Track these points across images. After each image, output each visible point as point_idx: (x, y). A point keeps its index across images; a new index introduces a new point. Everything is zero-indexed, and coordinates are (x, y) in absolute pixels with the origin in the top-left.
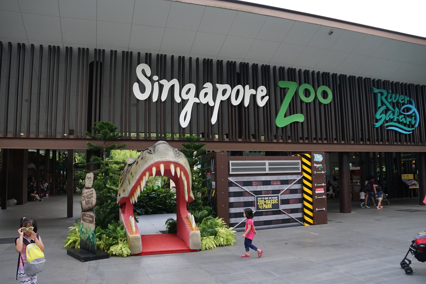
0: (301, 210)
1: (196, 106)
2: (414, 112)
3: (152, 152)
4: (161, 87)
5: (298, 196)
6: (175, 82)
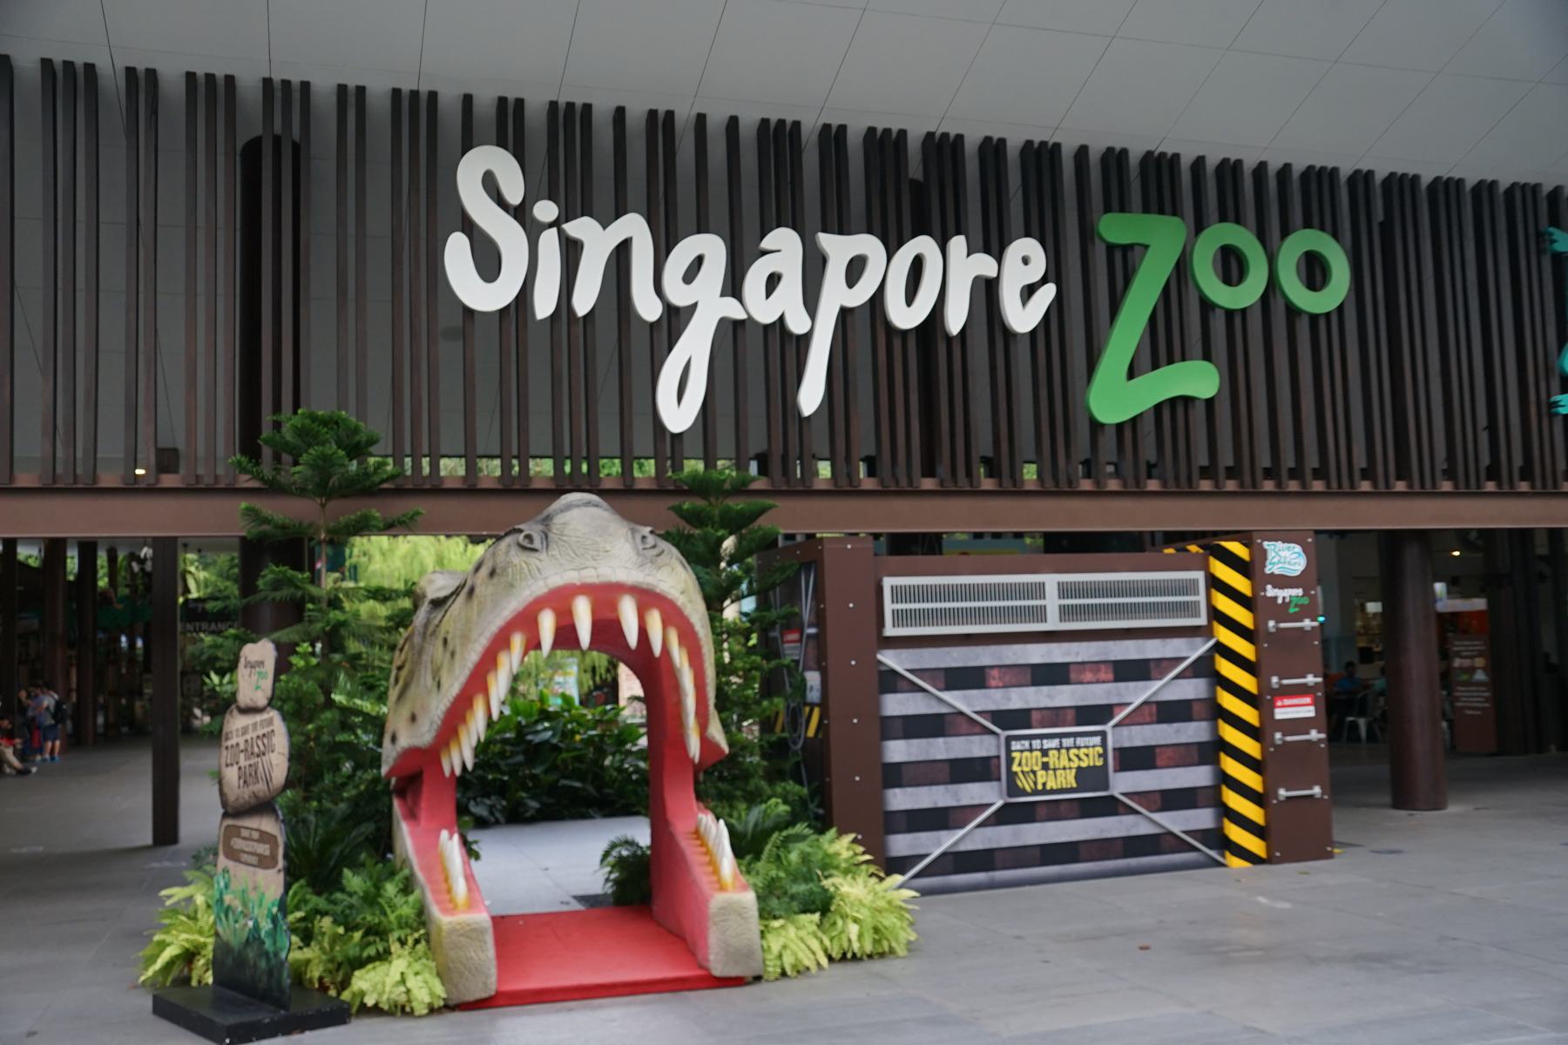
0: (1208, 797)
1: (732, 333)
3: (537, 544)
4: (571, 251)
5: (1194, 732)
6: (634, 226)
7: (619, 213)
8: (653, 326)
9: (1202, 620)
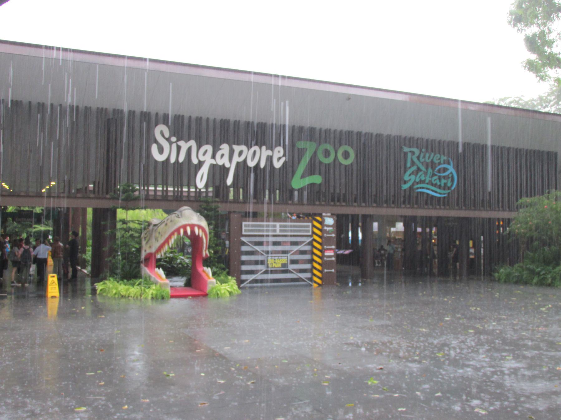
0: (311, 271)
1: (213, 167)
2: (451, 173)
3: (180, 216)
4: (179, 148)
5: (308, 257)
6: (192, 143)
7: (189, 139)
8: (196, 165)
9: (310, 233)
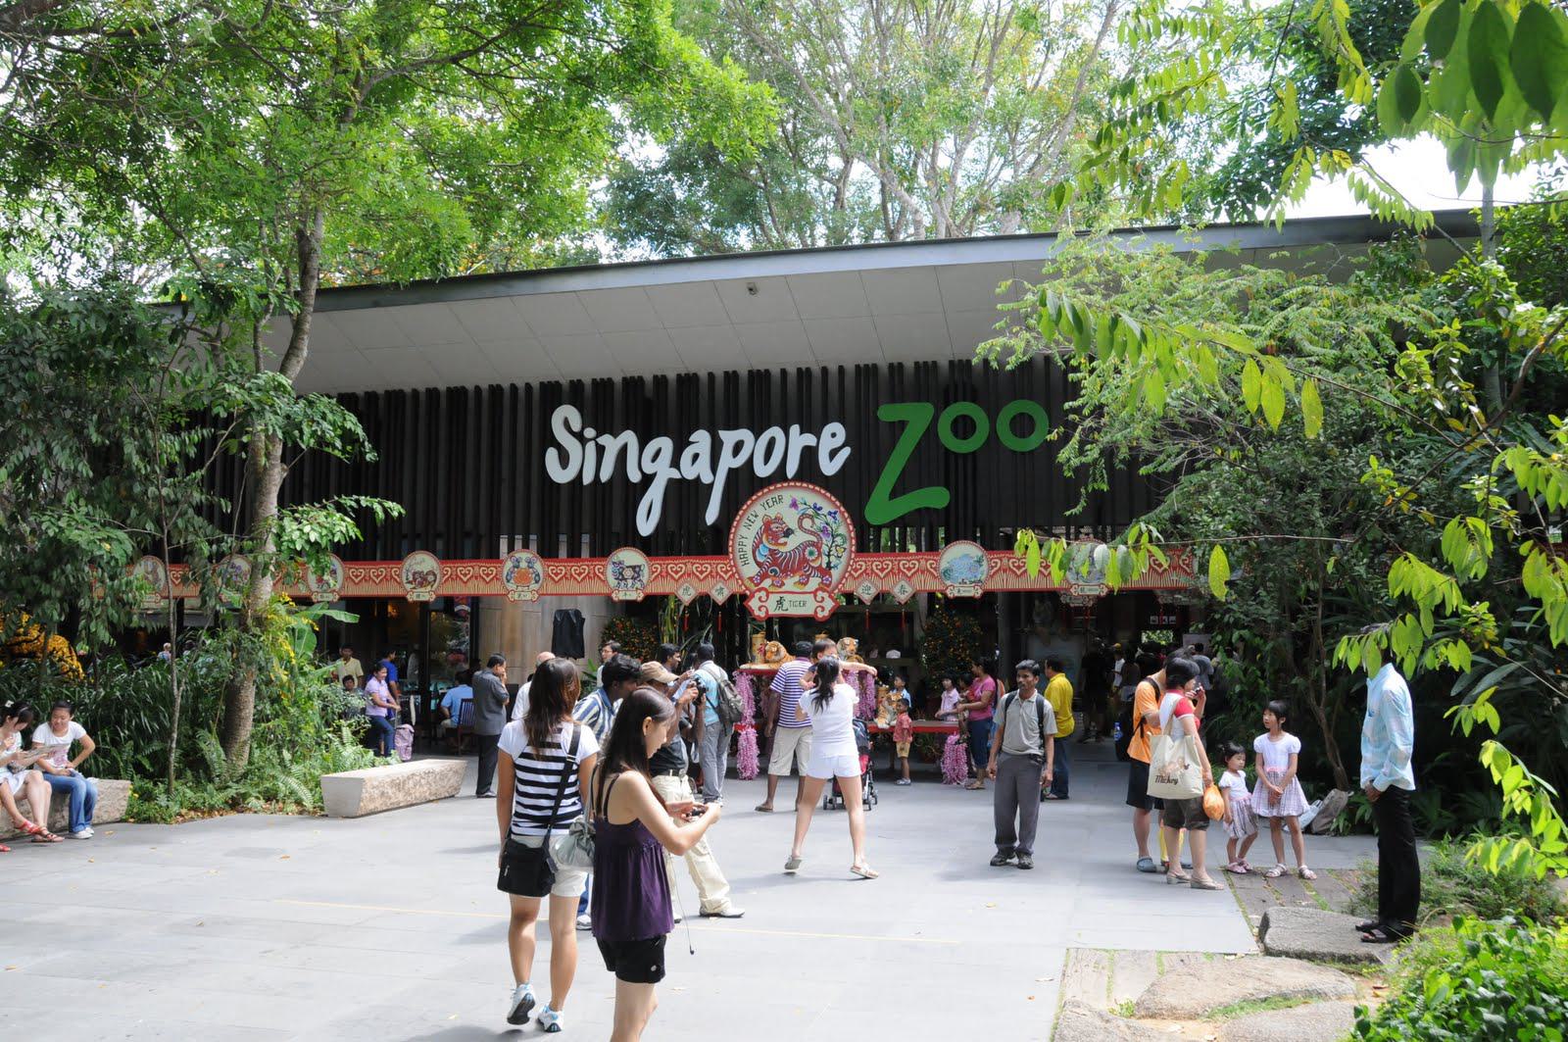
4: (601, 450)
6: (629, 437)
